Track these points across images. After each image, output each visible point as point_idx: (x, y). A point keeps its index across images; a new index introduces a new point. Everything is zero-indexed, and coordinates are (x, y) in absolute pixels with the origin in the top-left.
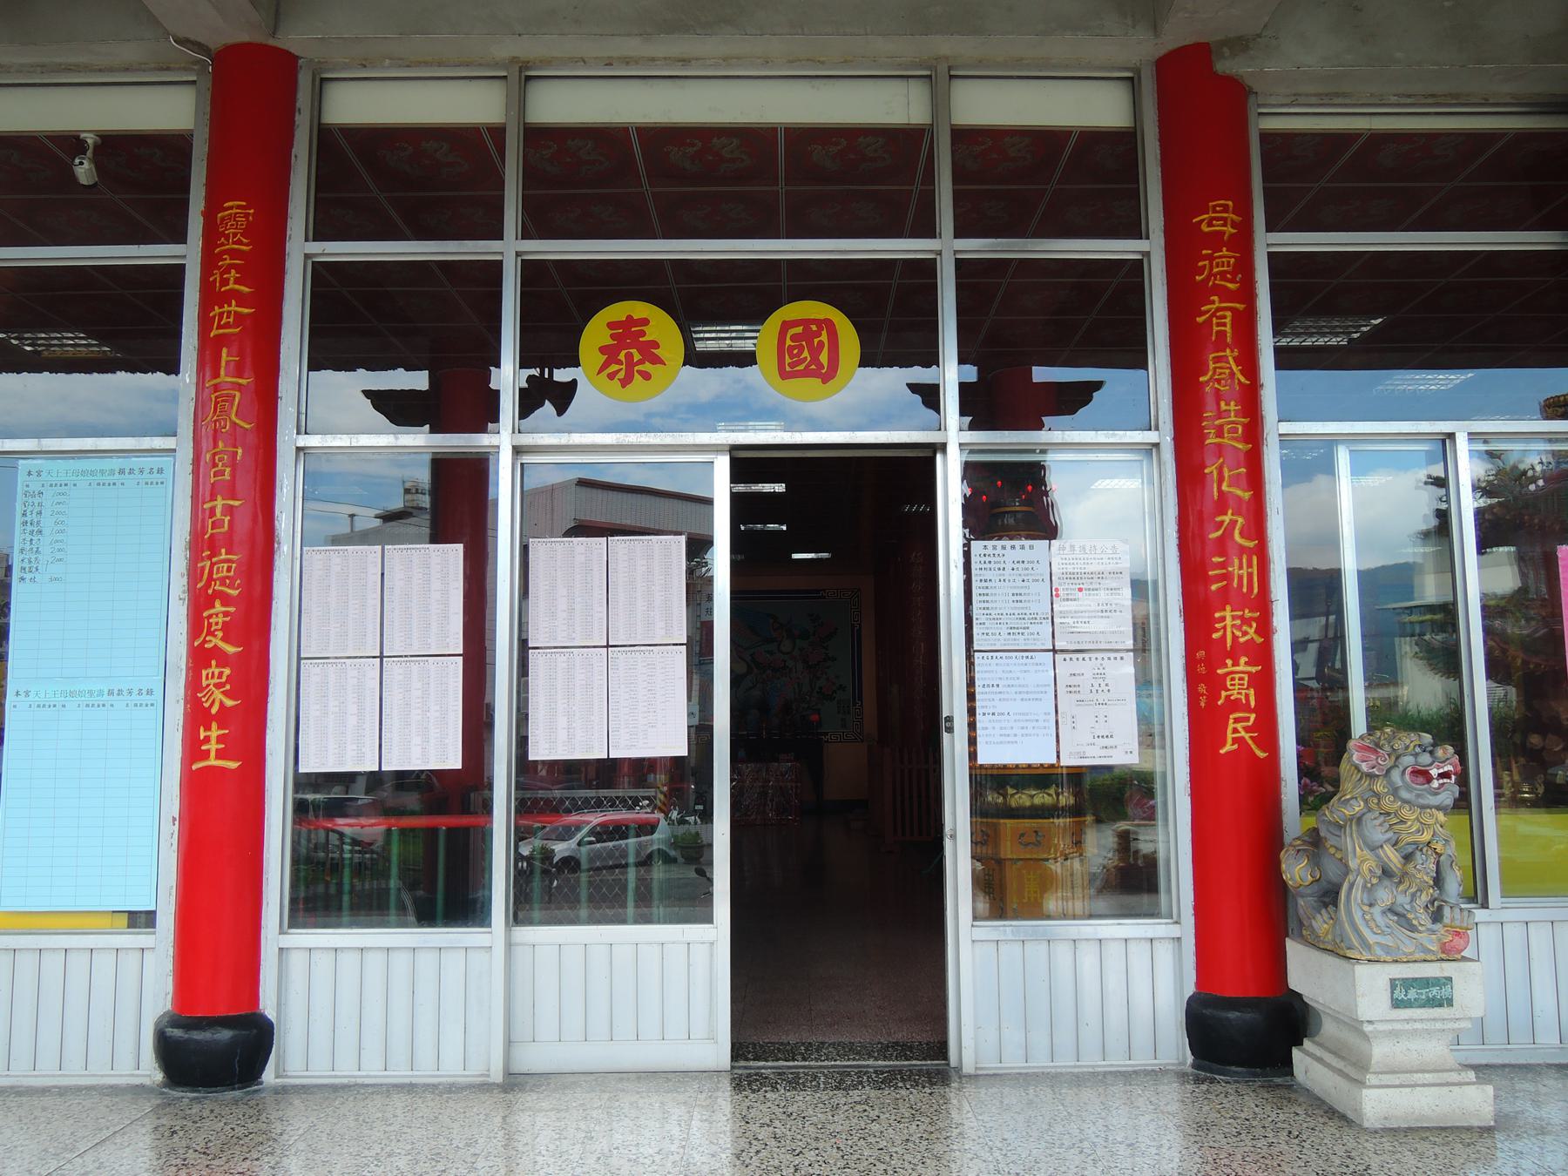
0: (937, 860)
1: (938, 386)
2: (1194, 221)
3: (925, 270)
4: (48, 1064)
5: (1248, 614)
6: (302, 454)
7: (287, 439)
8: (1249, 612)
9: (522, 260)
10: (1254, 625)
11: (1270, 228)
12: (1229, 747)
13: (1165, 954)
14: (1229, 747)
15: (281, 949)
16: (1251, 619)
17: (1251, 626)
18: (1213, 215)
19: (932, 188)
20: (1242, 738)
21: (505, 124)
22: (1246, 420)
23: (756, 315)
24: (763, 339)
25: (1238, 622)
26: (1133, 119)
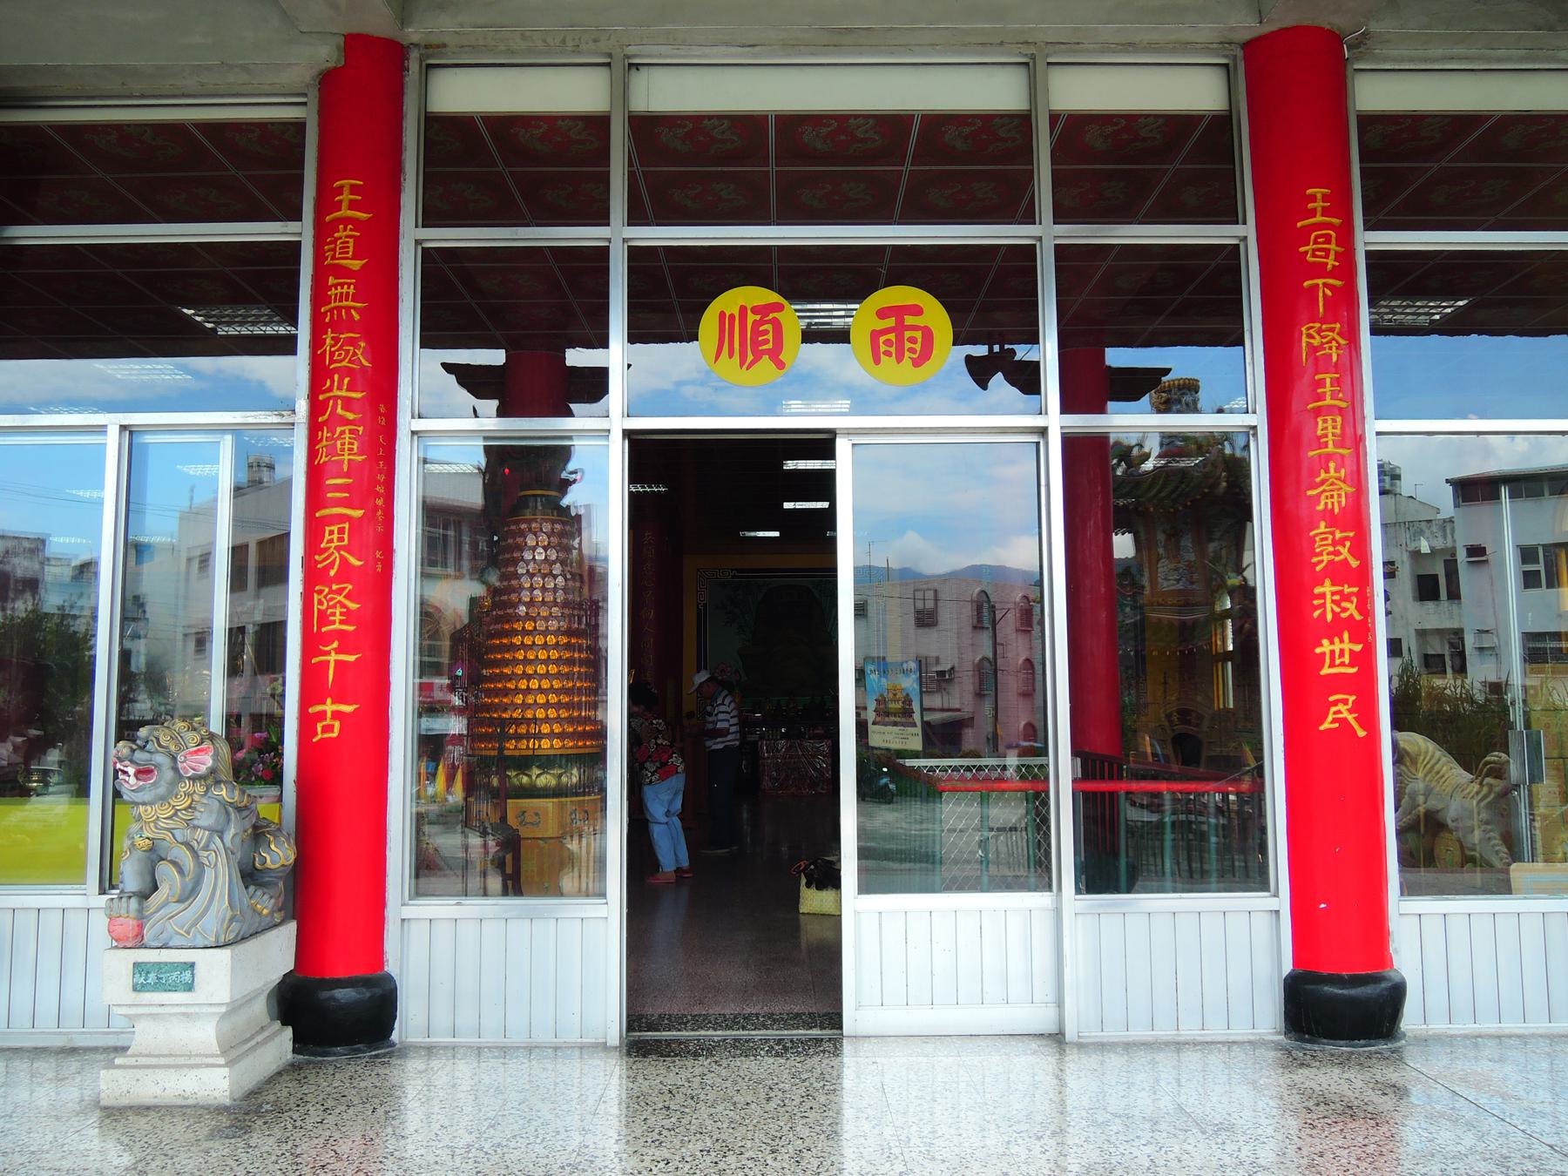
0: (198, 249)
1: (1038, 363)
2: (1299, 224)
3: (1025, 255)
4: (47, 1021)
5: (1347, 590)
6: (416, 437)
7: (406, 423)
8: (1349, 587)
9: (628, 246)
10: (1355, 600)
11: (1367, 228)
12: (1326, 725)
13: (1262, 923)
14: (1326, 725)
15: (403, 920)
16: (1352, 594)
17: (1344, 546)
18: (1316, 246)
19: (1030, 167)
20: (1345, 719)
21: (609, 112)
22: (1351, 490)
23: (858, 293)
24: (861, 316)
25: (1337, 597)
26: (1226, 99)
